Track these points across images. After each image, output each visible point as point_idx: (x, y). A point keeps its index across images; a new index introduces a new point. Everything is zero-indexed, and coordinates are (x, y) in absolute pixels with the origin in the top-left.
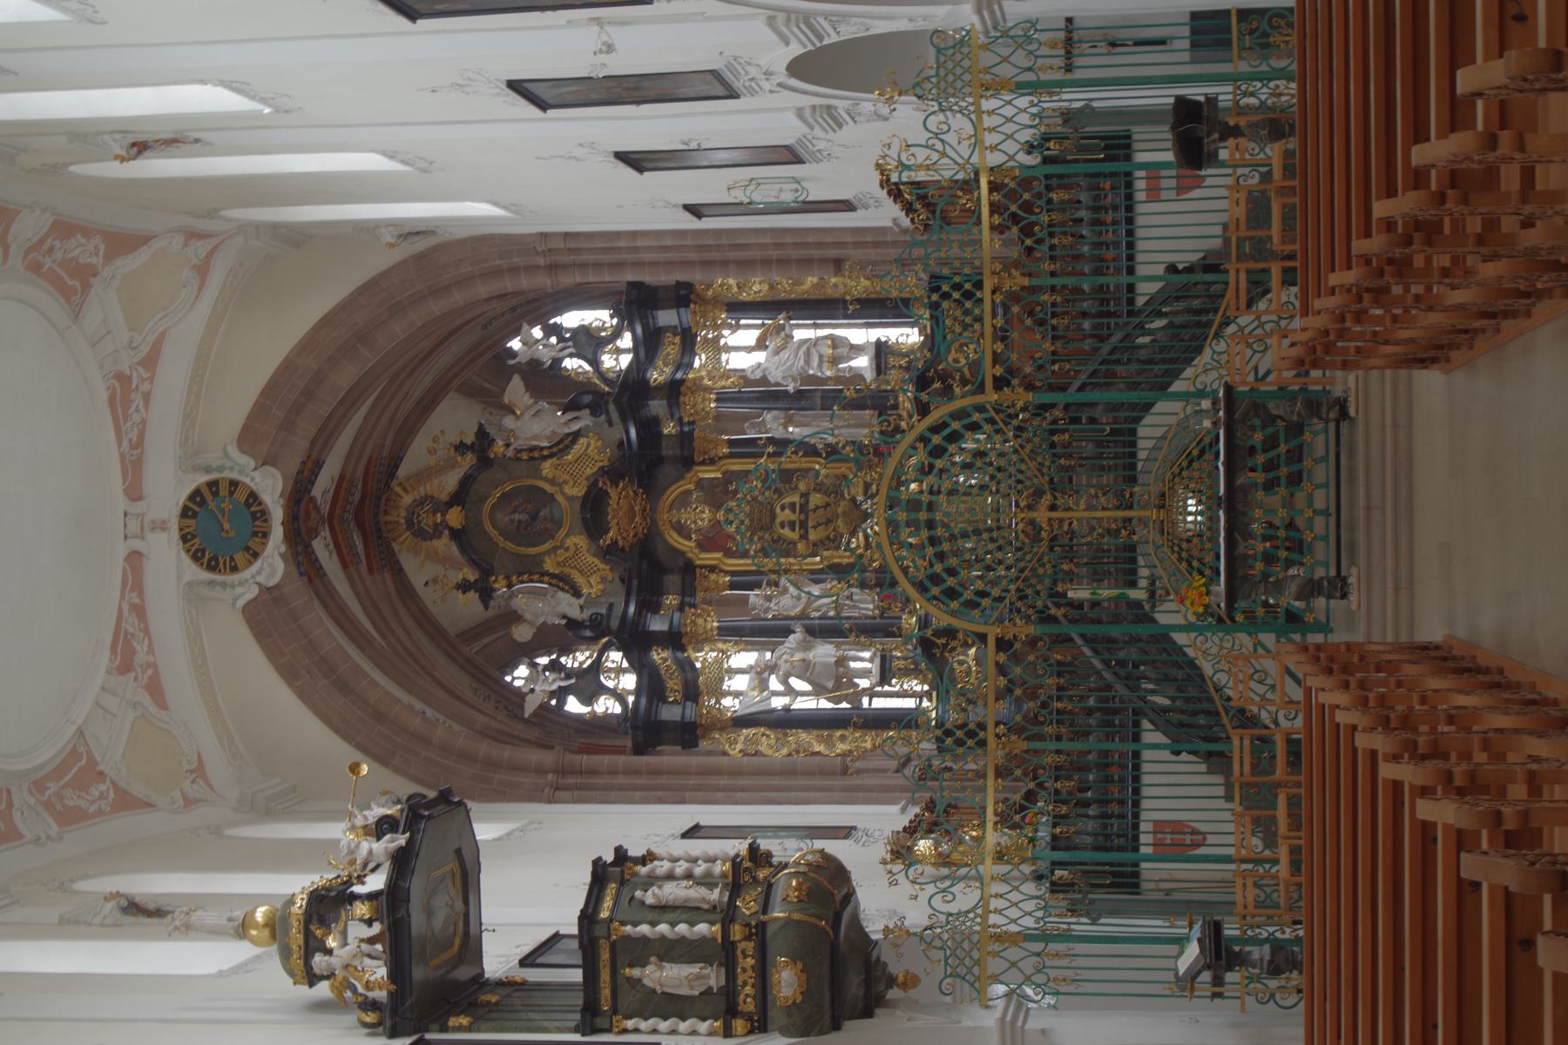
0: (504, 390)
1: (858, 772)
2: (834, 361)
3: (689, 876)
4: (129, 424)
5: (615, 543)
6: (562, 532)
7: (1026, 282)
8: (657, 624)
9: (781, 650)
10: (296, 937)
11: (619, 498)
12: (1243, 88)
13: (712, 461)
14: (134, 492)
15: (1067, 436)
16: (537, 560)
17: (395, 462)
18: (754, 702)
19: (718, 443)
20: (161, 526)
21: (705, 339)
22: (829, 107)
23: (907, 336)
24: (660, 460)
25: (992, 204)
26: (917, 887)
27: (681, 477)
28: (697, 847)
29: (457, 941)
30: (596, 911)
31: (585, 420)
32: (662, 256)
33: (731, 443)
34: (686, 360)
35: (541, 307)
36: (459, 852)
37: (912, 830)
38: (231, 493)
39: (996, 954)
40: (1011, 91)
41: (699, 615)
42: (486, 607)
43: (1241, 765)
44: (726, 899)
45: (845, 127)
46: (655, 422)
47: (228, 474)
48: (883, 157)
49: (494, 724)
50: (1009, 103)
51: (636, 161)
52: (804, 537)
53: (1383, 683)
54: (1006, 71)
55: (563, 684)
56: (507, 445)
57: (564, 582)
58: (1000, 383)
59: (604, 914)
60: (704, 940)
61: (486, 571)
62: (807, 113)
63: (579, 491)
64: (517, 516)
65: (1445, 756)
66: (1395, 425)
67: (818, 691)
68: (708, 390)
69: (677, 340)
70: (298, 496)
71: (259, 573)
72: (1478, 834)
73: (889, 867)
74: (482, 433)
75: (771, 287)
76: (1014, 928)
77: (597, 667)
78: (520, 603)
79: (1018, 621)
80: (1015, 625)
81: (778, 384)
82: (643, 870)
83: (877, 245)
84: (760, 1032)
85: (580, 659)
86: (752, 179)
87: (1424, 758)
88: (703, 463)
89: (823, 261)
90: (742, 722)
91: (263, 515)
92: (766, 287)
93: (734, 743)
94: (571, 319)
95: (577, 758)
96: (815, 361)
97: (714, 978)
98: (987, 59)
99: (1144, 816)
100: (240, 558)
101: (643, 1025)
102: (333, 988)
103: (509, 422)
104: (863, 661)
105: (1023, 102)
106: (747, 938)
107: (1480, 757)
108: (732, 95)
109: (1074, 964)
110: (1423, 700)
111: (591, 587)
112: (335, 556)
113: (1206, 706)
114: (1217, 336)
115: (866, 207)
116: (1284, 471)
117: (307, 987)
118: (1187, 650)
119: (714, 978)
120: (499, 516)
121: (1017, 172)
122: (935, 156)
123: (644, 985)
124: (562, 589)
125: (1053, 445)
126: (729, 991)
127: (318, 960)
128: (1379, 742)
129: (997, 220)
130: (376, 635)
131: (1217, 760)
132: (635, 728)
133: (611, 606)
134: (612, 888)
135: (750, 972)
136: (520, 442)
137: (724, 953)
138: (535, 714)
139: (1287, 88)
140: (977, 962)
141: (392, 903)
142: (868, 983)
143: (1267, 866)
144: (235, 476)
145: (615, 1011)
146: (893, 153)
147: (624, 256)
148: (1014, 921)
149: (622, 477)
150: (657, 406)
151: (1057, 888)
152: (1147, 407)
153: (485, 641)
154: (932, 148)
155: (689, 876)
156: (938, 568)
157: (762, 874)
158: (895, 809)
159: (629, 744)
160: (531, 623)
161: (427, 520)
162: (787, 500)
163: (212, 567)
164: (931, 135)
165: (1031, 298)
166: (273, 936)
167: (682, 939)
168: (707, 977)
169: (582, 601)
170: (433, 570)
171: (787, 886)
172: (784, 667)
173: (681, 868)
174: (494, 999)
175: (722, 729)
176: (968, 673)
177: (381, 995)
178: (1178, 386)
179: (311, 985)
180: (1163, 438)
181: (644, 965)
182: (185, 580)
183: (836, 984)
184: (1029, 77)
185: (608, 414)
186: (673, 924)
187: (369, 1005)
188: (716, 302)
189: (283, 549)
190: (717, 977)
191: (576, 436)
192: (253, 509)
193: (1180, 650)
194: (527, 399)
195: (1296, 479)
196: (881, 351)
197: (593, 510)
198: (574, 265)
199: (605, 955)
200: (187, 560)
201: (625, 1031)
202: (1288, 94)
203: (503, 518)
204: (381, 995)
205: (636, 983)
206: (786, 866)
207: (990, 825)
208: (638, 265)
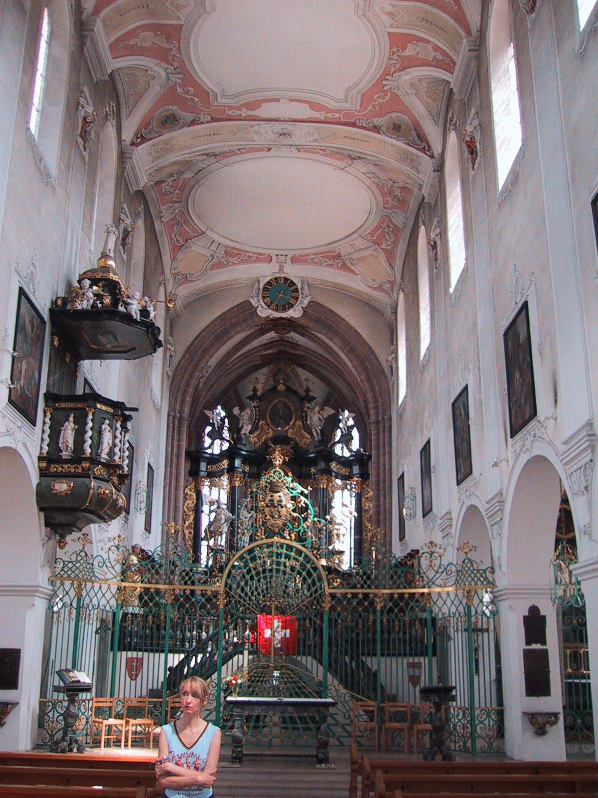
3: (115, 445)
4: (321, 258)
6: (273, 427)
7: (379, 608)
8: (237, 463)
9: (227, 511)
10: (99, 276)
12: (467, 712)
14: (294, 260)
15: (308, 625)
16: (264, 418)
17: (303, 367)
18: (206, 500)
20: (281, 270)
22: (451, 525)
24: (301, 466)
26: (107, 550)
30: (100, 403)
32: (381, 465)
34: (339, 476)
35: (360, 423)
38: (293, 298)
39: (72, 585)
40: (467, 604)
41: (240, 479)
42: (247, 398)
44: (102, 460)
45: (441, 533)
46: (316, 465)
47: (301, 296)
48: (435, 545)
50: (461, 603)
51: (426, 451)
55: (216, 426)
59: (99, 406)
60: (83, 451)
61: (260, 399)
62: (448, 516)
63: (290, 435)
64: (281, 411)
67: (211, 524)
68: (327, 486)
69: (347, 473)
70: (291, 324)
71: (262, 307)
73: (117, 538)
74: (313, 398)
76: (84, 593)
77: (223, 439)
78: (248, 411)
79: (226, 601)
80: (224, 599)
81: (329, 512)
84: (40, 474)
85: (226, 434)
86: (415, 497)
90: (199, 493)
91: (284, 309)
92: (367, 508)
94: (355, 433)
97: (65, 455)
99: (146, 654)
100: (268, 300)
101: (48, 420)
103: (317, 409)
105: (461, 609)
106: (83, 468)
109: (66, 620)
111: (253, 438)
112: (267, 341)
114: (352, 696)
117: (78, 279)
118: (210, 679)
119: (65, 455)
121: (428, 605)
122: (436, 569)
123: (65, 422)
124: (252, 427)
125: (304, 620)
126: (60, 461)
127: (87, 283)
129: (396, 596)
130: (237, 355)
134: (111, 410)
135: (68, 470)
136: (309, 413)
137: (78, 456)
139: (467, 732)
142: (61, 525)
143: (108, 713)
144: (300, 299)
145: (55, 409)
146: (438, 550)
147: (382, 450)
149: (294, 451)
150: (322, 465)
152: (320, 662)
154: (440, 567)
156: (253, 572)
157: (115, 479)
160: (240, 414)
164: (446, 567)
165: (371, 611)
168: (67, 451)
169: (248, 434)
170: (262, 379)
171: (107, 489)
172: (219, 511)
175: (196, 486)
177: (69, 307)
178: (330, 676)
180: (307, 669)
181: (74, 423)
184: (473, 613)
185: (320, 446)
187: (65, 301)
189: (271, 317)
190: (66, 455)
192: (287, 306)
194: (325, 416)
198: (378, 430)
200: (267, 279)
201: (45, 413)
202: (464, 733)
208: (378, 456)
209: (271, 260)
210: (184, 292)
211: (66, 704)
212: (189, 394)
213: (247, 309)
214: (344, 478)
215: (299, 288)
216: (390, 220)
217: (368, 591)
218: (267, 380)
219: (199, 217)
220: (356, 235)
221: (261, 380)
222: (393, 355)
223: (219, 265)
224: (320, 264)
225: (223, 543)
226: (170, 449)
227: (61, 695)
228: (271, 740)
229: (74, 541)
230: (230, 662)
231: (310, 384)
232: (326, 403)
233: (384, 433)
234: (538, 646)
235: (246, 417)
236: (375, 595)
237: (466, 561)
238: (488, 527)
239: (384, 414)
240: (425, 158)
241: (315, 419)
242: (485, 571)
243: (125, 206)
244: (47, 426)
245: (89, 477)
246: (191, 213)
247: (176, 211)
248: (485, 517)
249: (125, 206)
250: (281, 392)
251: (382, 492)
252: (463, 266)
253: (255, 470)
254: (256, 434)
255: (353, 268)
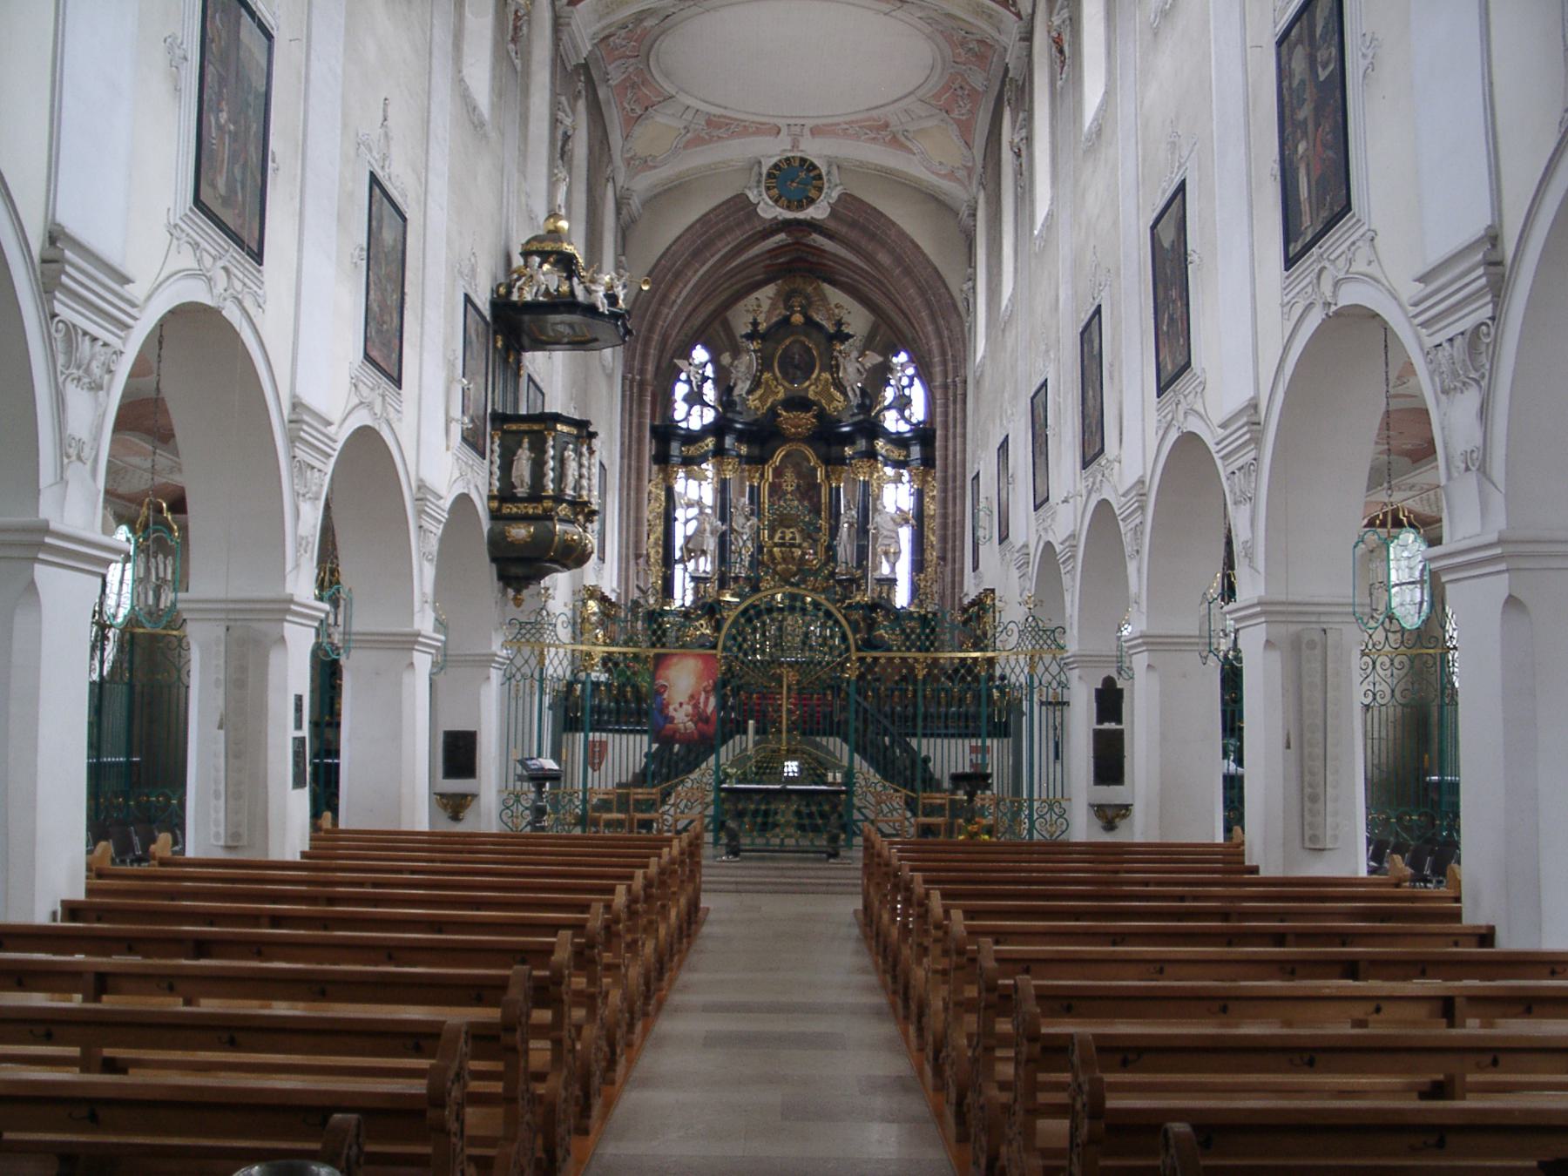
0: (873, 351)
1: (637, 564)
2: (886, 554)
3: (581, 476)
5: (780, 415)
6: (786, 384)
7: (920, 677)
8: (729, 441)
10: (548, 247)
11: (807, 419)
13: (828, 477)
14: (816, 132)
17: (833, 283)
19: (838, 480)
20: (795, 146)
21: (902, 475)
23: (902, 598)
24: (829, 444)
25: (965, 659)
27: (818, 457)
28: (596, 470)
29: (544, 338)
31: (855, 401)
33: (838, 489)
35: (924, 373)
36: (596, 340)
37: (603, 599)
39: (532, 652)
42: (742, 336)
43: (640, 793)
46: (852, 443)
47: (826, 185)
49: (670, 341)
51: (1004, 447)
52: (776, 545)
53: (683, 871)
54: (1040, 669)
56: (840, 352)
57: (756, 384)
58: (861, 660)
59: (559, 427)
60: (543, 488)
61: (764, 337)
62: (1024, 551)
63: (811, 395)
65: (630, 919)
66: (828, 885)
67: (688, 539)
68: (871, 476)
70: (812, 226)
71: (766, 203)
72: (581, 936)
74: (848, 336)
75: (933, 516)
76: (547, 662)
82: (584, 449)
83: (953, 582)
87: (645, 890)
88: (827, 471)
89: (944, 550)
90: (670, 492)
91: (801, 207)
93: (656, 486)
95: (649, 394)
96: (886, 542)
97: (521, 491)
98: (1047, 658)
99: (610, 735)
100: (775, 192)
101: (496, 447)
102: (519, 267)
103: (854, 354)
104: (705, 565)
105: (1022, 679)
107: (629, 938)
108: (1036, 508)
110: (674, 893)
113: (673, 774)
115: (975, 578)
116: (806, 822)
119: (521, 491)
120: (798, 345)
126: (514, 499)
128: (653, 869)
131: (641, 779)
132: (666, 427)
133: (740, 413)
137: (536, 495)
138: (675, 365)
140: (528, 641)
141: (567, 304)
142: (517, 578)
144: (825, 190)
145: (505, 432)
147: (951, 430)
148: (551, 662)
150: (862, 444)
151: (570, 685)
152: (845, 740)
153: (722, 334)
155: (581, 476)
157: (580, 517)
158: (615, 585)
159: (657, 423)
160: (731, 364)
161: (796, 302)
162: (798, 536)
163: (770, 175)
166: (550, 232)
167: (544, 475)
170: (766, 305)
171: (574, 532)
173: (585, 471)
174: (511, 360)
175: (664, 480)
176: (696, 629)
177: (515, 297)
179: (521, 254)
180: (836, 758)
182: (763, 160)
183: (520, 560)
184: (1036, 683)
186: (553, 470)
188: (924, 482)
189: (780, 218)
191: (844, 393)
193: (705, 759)
194: (868, 365)
195: (802, 827)
196: (891, 582)
197: (798, 403)
198: (947, 399)
199: (536, 427)
200: (775, 160)
203: (796, 348)
204: (515, 297)
205: (520, 445)
206: (585, 531)
207: (606, 649)
209: (778, 133)
210: (642, 184)
211: (532, 796)
212: (654, 343)
213: (740, 207)
214: (899, 465)
215: (824, 174)
216: (964, 79)
217: (907, 654)
218: (773, 307)
219: (667, 75)
220: (912, 98)
221: (762, 305)
222: (970, 283)
223: (698, 141)
224: (857, 137)
225: (709, 568)
226: (627, 431)
227: (525, 785)
228: (782, 840)
229: (532, 596)
230: (731, 742)
231: (843, 313)
232: (869, 344)
233: (955, 402)
234: (1112, 726)
235: (743, 369)
236: (916, 660)
237: (1030, 619)
238: (1224, 479)
239: (956, 369)
240: (1008, 16)
241: (852, 372)
242: (1053, 631)
243: (563, 99)
244: (496, 455)
245: (551, 519)
246: (654, 72)
247: (630, 70)
248: (1216, 456)
249: (563, 99)
250: (797, 326)
251: (950, 494)
252: (1103, 90)
253: (756, 451)
254: (759, 392)
255: (908, 144)
